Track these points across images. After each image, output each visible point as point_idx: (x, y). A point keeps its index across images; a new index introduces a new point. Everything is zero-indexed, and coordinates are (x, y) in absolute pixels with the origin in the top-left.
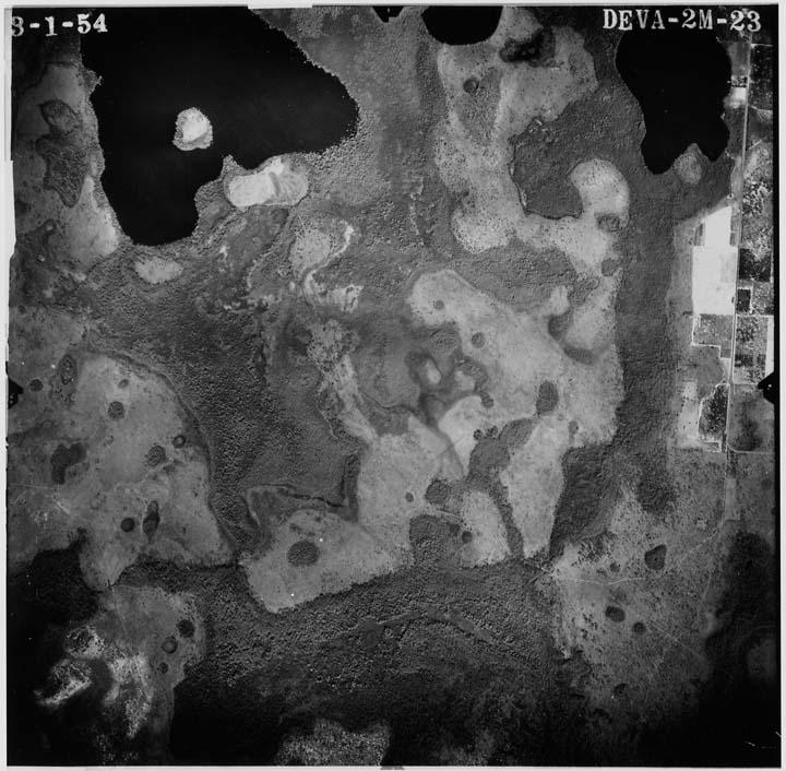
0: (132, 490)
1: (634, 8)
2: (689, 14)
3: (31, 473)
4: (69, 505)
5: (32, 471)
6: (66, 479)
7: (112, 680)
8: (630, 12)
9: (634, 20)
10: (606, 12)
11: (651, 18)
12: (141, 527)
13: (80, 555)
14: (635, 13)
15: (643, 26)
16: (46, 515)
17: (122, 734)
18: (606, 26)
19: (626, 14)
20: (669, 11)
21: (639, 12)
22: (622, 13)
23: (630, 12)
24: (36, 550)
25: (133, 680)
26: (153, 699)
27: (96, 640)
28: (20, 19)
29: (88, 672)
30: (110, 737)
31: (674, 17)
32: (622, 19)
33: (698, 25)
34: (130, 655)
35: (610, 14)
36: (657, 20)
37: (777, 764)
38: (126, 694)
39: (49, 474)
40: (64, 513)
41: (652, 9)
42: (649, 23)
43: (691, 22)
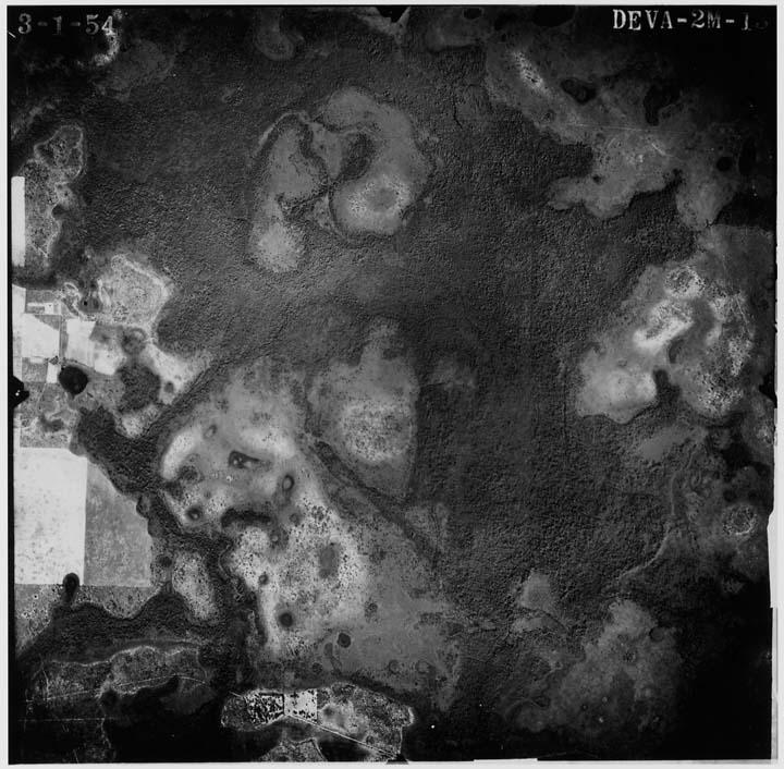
0: (727, 130)
1: (642, 8)
2: (699, 15)
3: (624, 116)
4: (663, 145)
5: (625, 113)
6: (660, 120)
7: (714, 319)
8: (639, 13)
9: (643, 20)
10: (616, 12)
11: (660, 20)
12: (737, 166)
13: (677, 196)
14: (644, 14)
15: (652, 26)
16: (641, 157)
17: (725, 372)
18: (616, 26)
19: (634, 15)
20: (677, 11)
21: (648, 12)
22: (631, 13)
23: (639, 13)
24: (633, 191)
25: (735, 318)
26: (755, 336)
27: (697, 280)
28: (28, 16)
29: (689, 312)
30: (715, 375)
31: (682, 17)
32: (631, 19)
33: (706, 24)
34: (731, 294)
35: (620, 14)
36: (666, 20)
37: (762, 751)
38: (728, 332)
39: (642, 117)
40: (659, 155)
41: (662, 8)
42: (657, 24)
43: (700, 23)
